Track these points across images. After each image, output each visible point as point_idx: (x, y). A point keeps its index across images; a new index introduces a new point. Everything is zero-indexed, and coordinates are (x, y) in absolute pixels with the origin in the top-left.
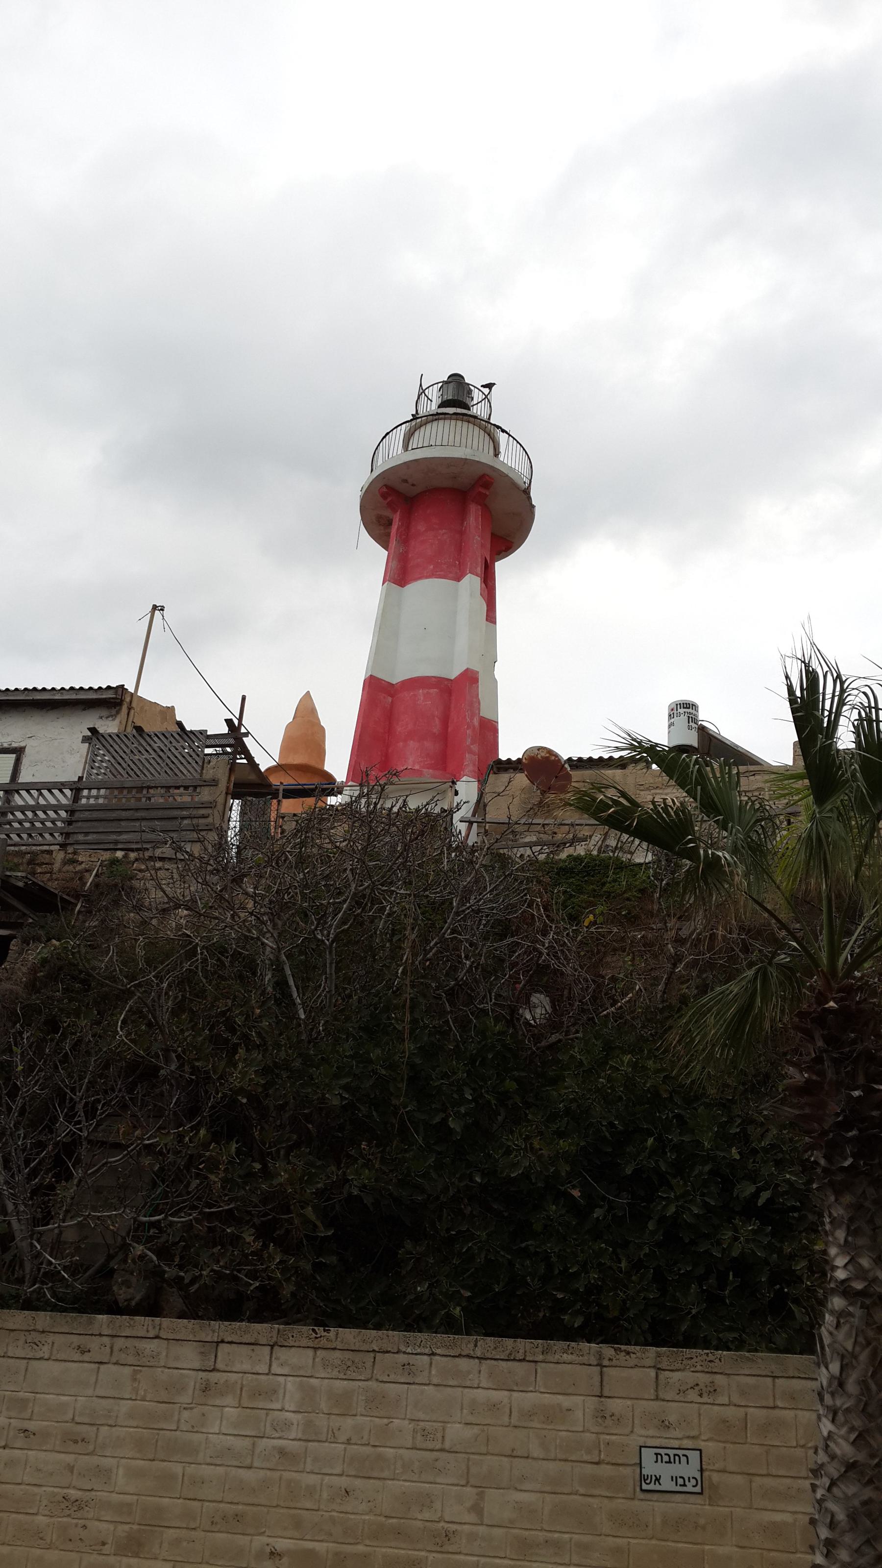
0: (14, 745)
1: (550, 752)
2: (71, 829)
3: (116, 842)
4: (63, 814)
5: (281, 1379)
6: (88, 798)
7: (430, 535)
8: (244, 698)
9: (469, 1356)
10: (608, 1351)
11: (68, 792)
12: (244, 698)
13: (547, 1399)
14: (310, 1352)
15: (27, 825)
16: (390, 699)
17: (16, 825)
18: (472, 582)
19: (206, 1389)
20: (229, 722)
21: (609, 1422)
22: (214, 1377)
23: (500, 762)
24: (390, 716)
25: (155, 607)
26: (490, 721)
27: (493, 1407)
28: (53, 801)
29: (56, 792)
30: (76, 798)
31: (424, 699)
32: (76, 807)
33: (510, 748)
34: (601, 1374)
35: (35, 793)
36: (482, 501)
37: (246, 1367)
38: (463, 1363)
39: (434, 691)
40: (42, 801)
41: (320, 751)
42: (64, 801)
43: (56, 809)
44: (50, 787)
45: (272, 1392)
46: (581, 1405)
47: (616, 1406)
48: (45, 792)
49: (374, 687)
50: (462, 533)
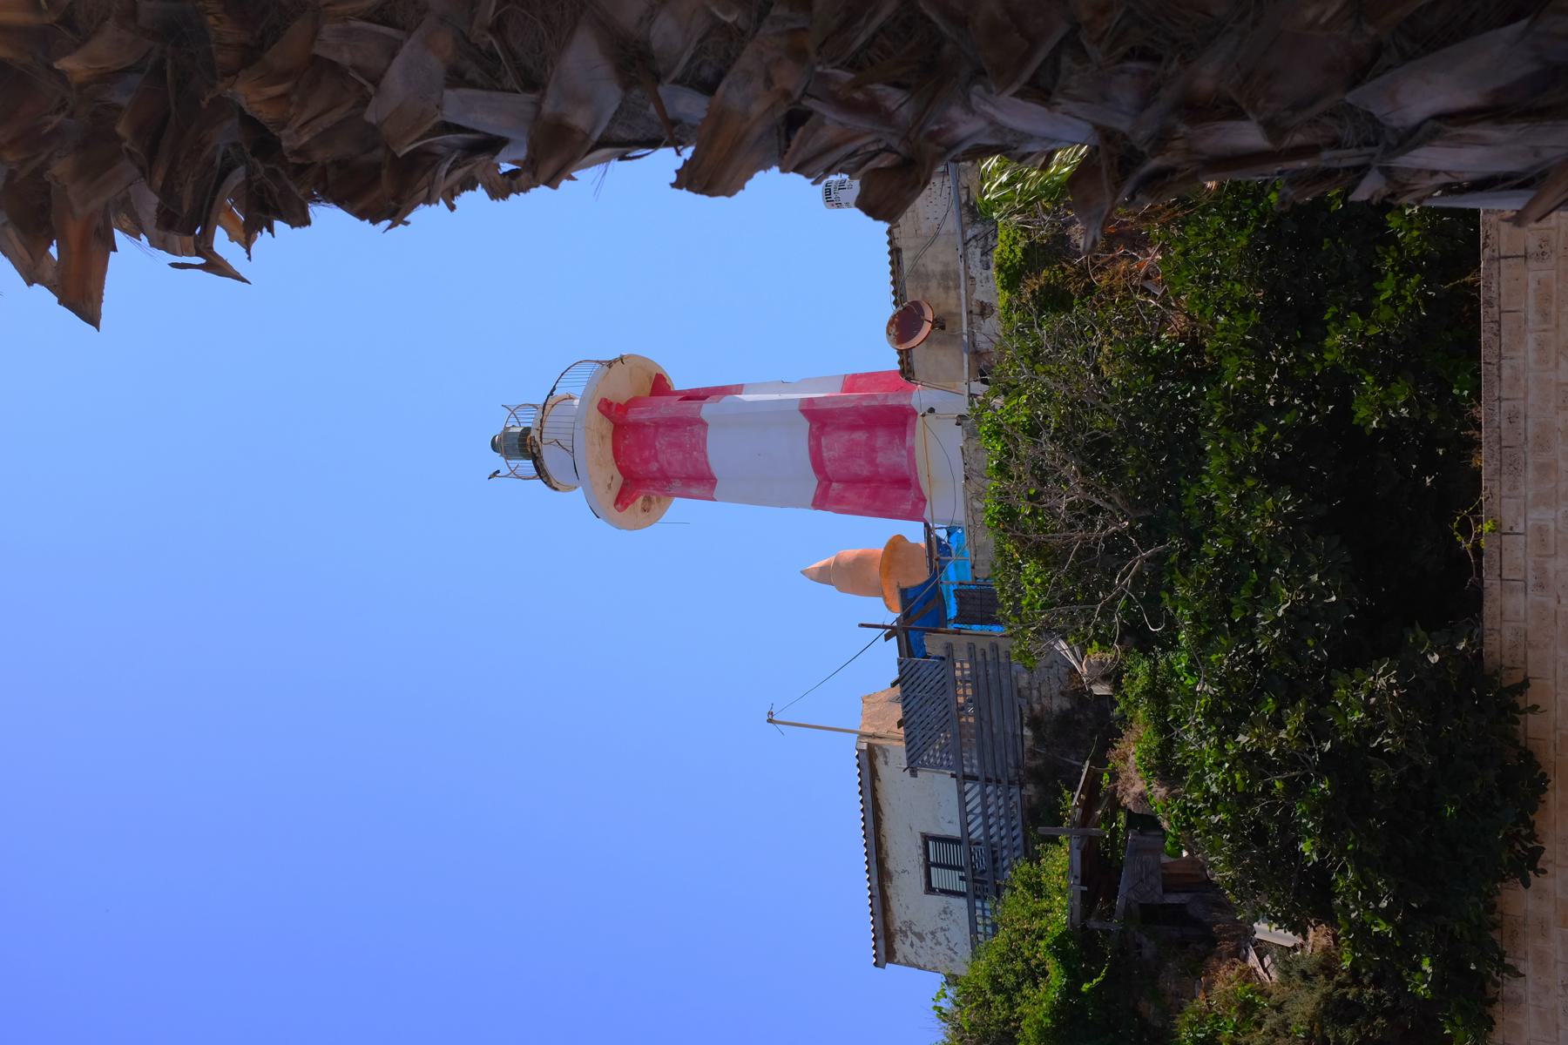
0: (920, 842)
1: (891, 323)
2: (1005, 782)
3: (1014, 735)
4: (989, 789)
5: (1530, 523)
6: (972, 766)
7: (666, 454)
8: (862, 625)
9: (1499, 369)
10: (1485, 254)
11: (968, 786)
12: (862, 625)
13: (1531, 301)
14: (1505, 501)
15: (1003, 822)
16: (834, 485)
17: (1003, 832)
18: (707, 410)
19: (1541, 586)
20: (887, 637)
21: (1546, 249)
22: (1531, 581)
23: (902, 372)
24: (852, 481)
25: (770, 721)
26: (844, 383)
27: (1541, 345)
28: (978, 800)
29: (968, 798)
30: (973, 778)
31: (835, 445)
32: (982, 778)
33: (888, 360)
34: (1506, 257)
35: (970, 817)
36: (624, 408)
37: (1520, 554)
38: (1506, 372)
39: (824, 441)
40: (978, 810)
41: (860, 563)
42: (977, 788)
43: (985, 797)
44: (963, 804)
45: (1541, 530)
46: (1534, 273)
47: (1533, 245)
48: (969, 808)
49: (822, 501)
50: (657, 425)
